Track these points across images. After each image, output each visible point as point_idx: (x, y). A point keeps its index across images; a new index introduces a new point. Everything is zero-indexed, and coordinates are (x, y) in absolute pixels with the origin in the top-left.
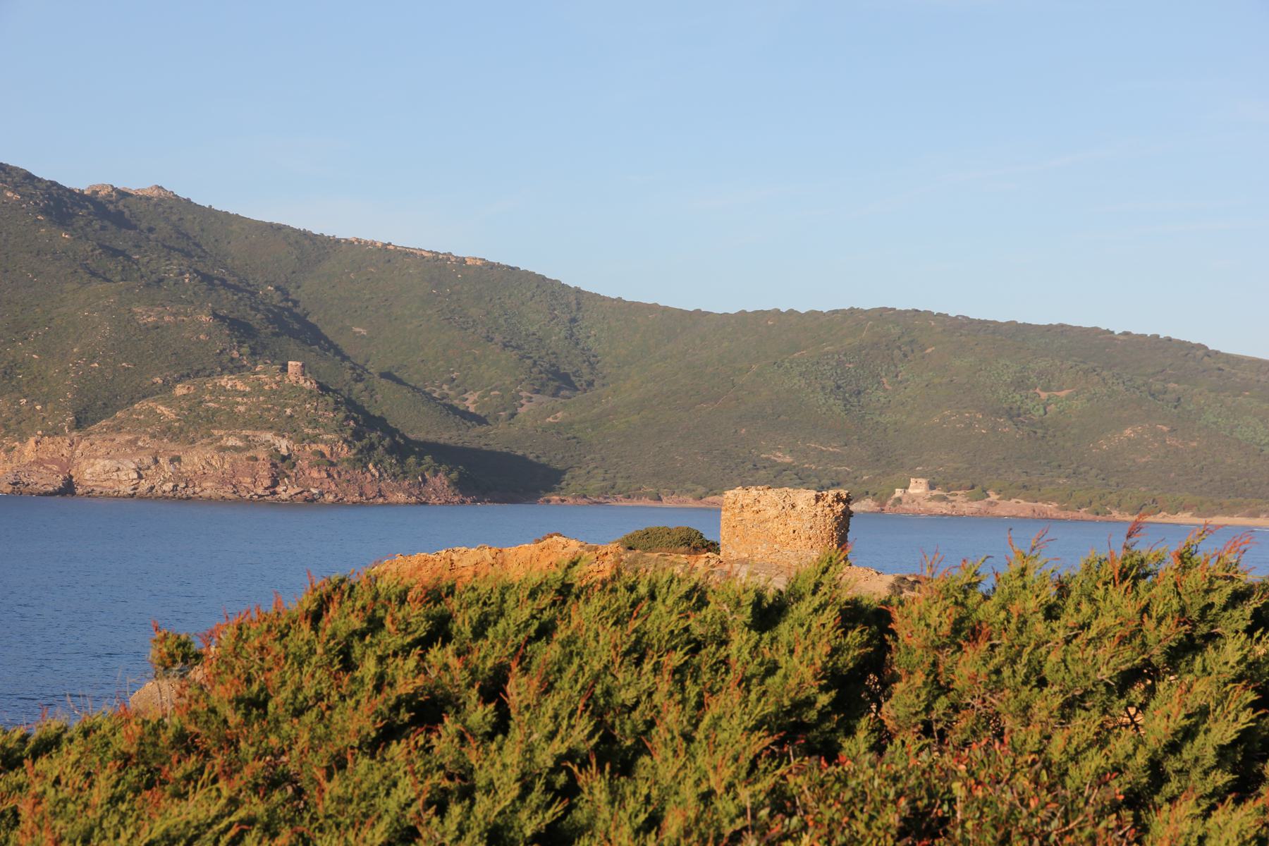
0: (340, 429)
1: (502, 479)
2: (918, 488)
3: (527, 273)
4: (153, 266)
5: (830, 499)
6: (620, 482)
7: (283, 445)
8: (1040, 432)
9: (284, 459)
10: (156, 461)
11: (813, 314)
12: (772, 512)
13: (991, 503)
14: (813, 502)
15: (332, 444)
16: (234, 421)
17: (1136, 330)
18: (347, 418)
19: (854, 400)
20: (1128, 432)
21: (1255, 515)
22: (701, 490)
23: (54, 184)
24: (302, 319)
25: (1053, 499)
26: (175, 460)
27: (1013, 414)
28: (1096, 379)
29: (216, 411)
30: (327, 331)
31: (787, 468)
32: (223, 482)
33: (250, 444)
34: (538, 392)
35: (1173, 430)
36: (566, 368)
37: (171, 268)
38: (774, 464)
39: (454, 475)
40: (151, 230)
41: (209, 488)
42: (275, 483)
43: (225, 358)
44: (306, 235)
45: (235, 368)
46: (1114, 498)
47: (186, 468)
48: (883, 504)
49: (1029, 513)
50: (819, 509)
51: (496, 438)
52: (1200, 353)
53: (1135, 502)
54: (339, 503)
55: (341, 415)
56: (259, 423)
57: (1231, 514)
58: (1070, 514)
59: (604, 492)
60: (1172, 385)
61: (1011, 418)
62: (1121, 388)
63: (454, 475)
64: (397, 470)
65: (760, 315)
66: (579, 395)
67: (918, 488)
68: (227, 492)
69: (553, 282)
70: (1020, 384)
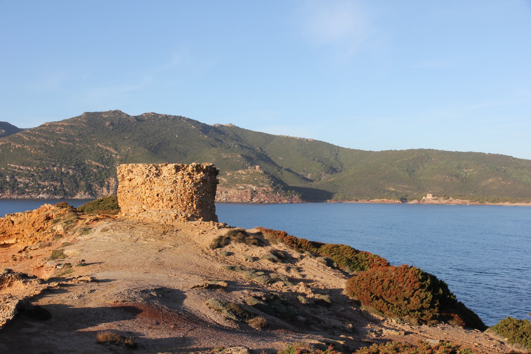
0: (270, 183)
1: (314, 195)
2: (429, 196)
3: (324, 142)
4: (228, 143)
5: (190, 169)
6: (347, 196)
7: (254, 188)
8: (465, 181)
9: (254, 191)
10: (221, 193)
11: (401, 151)
13: (450, 200)
14: (174, 171)
15: (267, 187)
16: (241, 182)
17: (492, 153)
18: (271, 180)
20: (490, 180)
21: (528, 202)
22: (369, 198)
23: (204, 124)
24: (266, 156)
25: (468, 199)
26: (226, 192)
27: (457, 176)
29: (237, 179)
30: (272, 159)
31: (393, 192)
32: (238, 198)
33: (246, 188)
34: (327, 173)
35: (503, 179)
36: (334, 167)
37: (232, 144)
38: (389, 191)
39: (300, 195)
40: (228, 135)
41: (235, 200)
42: (252, 198)
43: (244, 166)
44: (267, 134)
45: (244, 168)
46: (486, 198)
47: (229, 195)
48: (419, 201)
49: (461, 203)
50: (179, 177)
51: (314, 185)
52: (511, 158)
53: (492, 199)
54: (269, 203)
55: (270, 180)
56: (248, 182)
57: (521, 202)
58: (473, 203)
59: (342, 199)
60: (503, 167)
61: (456, 177)
62: (488, 168)
63: (300, 195)
64: (285, 194)
66: (338, 174)
67: (429, 196)
68: (240, 201)
69: (332, 145)
70: (459, 168)
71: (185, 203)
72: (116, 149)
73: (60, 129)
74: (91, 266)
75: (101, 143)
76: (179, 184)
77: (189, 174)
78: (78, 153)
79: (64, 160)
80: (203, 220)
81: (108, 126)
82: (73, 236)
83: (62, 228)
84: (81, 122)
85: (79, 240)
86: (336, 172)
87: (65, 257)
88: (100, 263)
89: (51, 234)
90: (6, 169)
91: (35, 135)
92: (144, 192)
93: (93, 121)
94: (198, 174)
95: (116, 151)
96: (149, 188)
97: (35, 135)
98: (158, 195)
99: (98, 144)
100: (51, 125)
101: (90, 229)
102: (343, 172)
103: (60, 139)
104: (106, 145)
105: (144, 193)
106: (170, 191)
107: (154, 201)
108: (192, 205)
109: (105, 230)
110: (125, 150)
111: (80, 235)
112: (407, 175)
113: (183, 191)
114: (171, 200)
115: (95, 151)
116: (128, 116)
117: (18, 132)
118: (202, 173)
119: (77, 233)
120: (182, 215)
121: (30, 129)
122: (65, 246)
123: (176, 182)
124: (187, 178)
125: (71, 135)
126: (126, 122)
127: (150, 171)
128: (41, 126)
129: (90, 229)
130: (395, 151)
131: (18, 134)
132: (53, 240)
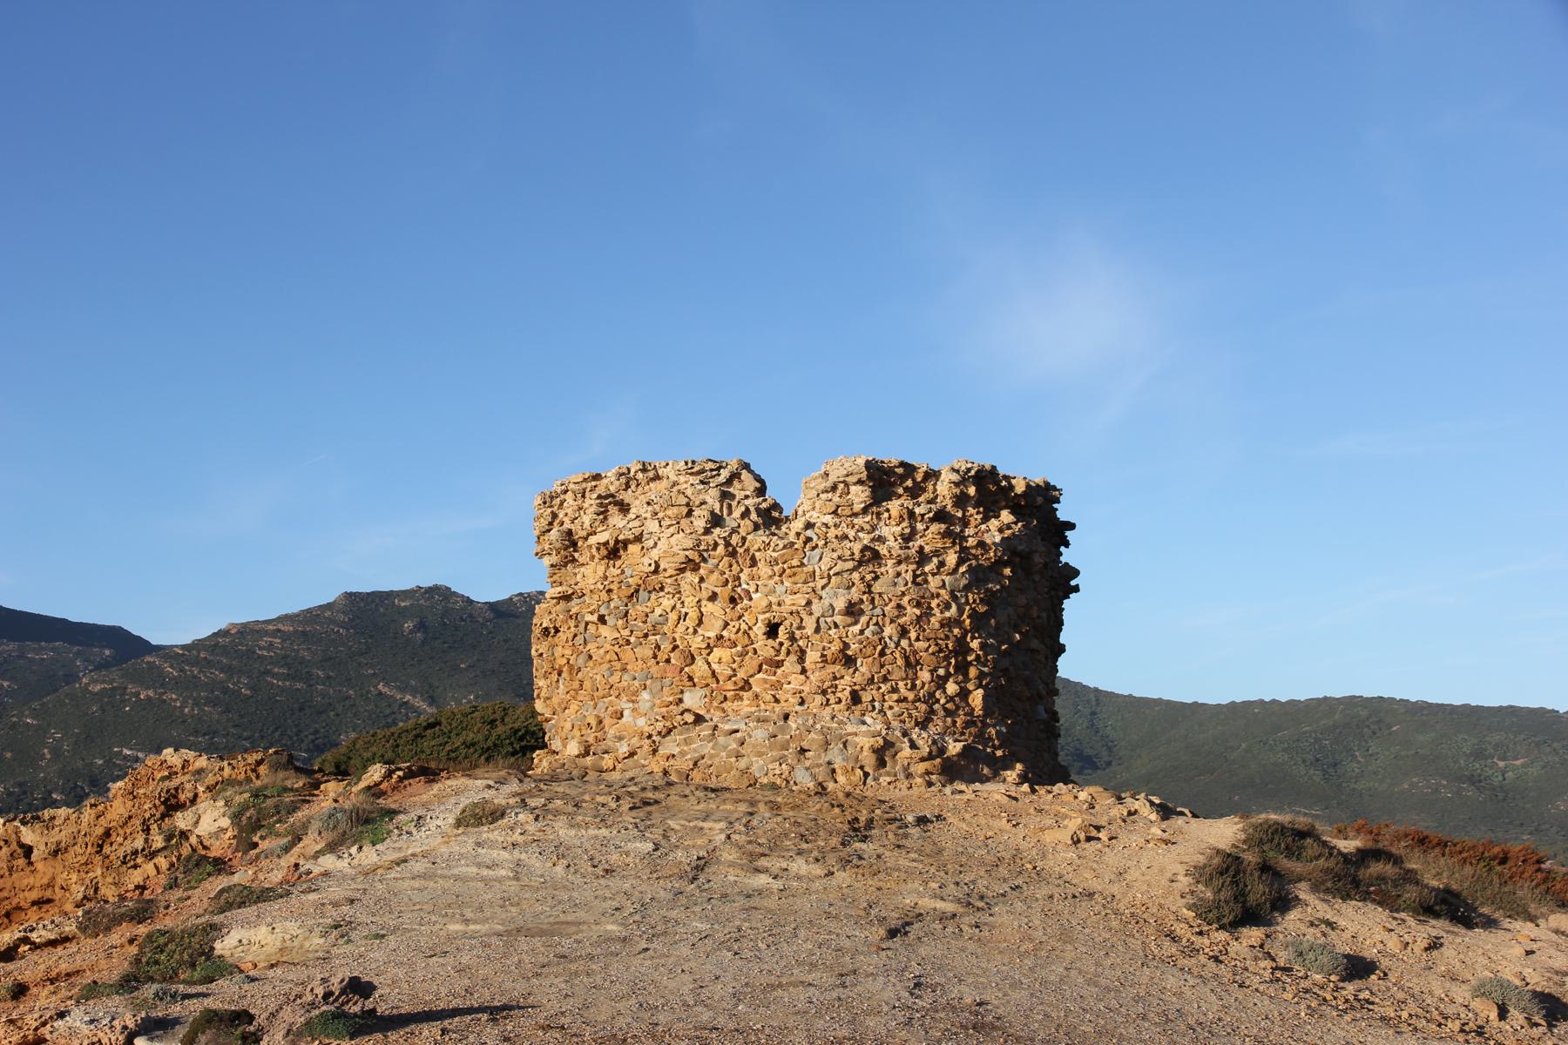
11: (1292, 702)
12: (670, 545)
14: (859, 495)
19: (1331, 770)
27: (1474, 780)
28: (1548, 750)
36: (1088, 752)
65: (1247, 704)
70: (1479, 754)
71: (925, 676)
72: (432, 701)
73: (271, 644)
74: (429, 1031)
75: (387, 684)
76: (889, 567)
77: (941, 516)
78: (320, 713)
79: (277, 735)
80: (1023, 778)
81: (411, 632)
82: (289, 859)
83: (225, 822)
84: (331, 621)
85: (326, 874)
86: (1095, 767)
87: (222, 969)
88: (496, 1012)
89: (161, 861)
90: (109, 762)
91: (196, 662)
92: (693, 614)
93: (366, 614)
94: (985, 519)
95: (430, 705)
96: (724, 593)
97: (196, 662)
98: (772, 630)
99: (380, 687)
100: (248, 631)
101: (392, 813)
102: (1114, 768)
103: (267, 672)
104: (403, 690)
105: (690, 622)
106: (840, 604)
107: (751, 663)
108: (964, 694)
109: (481, 816)
110: (459, 703)
111: (332, 848)
112: (1317, 776)
113: (912, 612)
114: (849, 661)
115: (371, 707)
116: (469, 601)
117: (149, 653)
118: (1006, 516)
119: (312, 843)
120: (913, 746)
121: (183, 647)
122: (229, 906)
123: (876, 556)
124: (930, 537)
125: (302, 661)
126: (462, 619)
127: (725, 496)
128: (214, 634)
129: (392, 813)
130: (1274, 701)
131: (148, 659)
132: (173, 885)
